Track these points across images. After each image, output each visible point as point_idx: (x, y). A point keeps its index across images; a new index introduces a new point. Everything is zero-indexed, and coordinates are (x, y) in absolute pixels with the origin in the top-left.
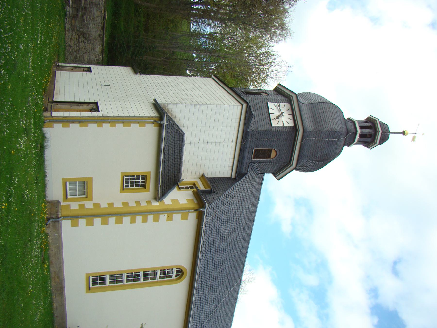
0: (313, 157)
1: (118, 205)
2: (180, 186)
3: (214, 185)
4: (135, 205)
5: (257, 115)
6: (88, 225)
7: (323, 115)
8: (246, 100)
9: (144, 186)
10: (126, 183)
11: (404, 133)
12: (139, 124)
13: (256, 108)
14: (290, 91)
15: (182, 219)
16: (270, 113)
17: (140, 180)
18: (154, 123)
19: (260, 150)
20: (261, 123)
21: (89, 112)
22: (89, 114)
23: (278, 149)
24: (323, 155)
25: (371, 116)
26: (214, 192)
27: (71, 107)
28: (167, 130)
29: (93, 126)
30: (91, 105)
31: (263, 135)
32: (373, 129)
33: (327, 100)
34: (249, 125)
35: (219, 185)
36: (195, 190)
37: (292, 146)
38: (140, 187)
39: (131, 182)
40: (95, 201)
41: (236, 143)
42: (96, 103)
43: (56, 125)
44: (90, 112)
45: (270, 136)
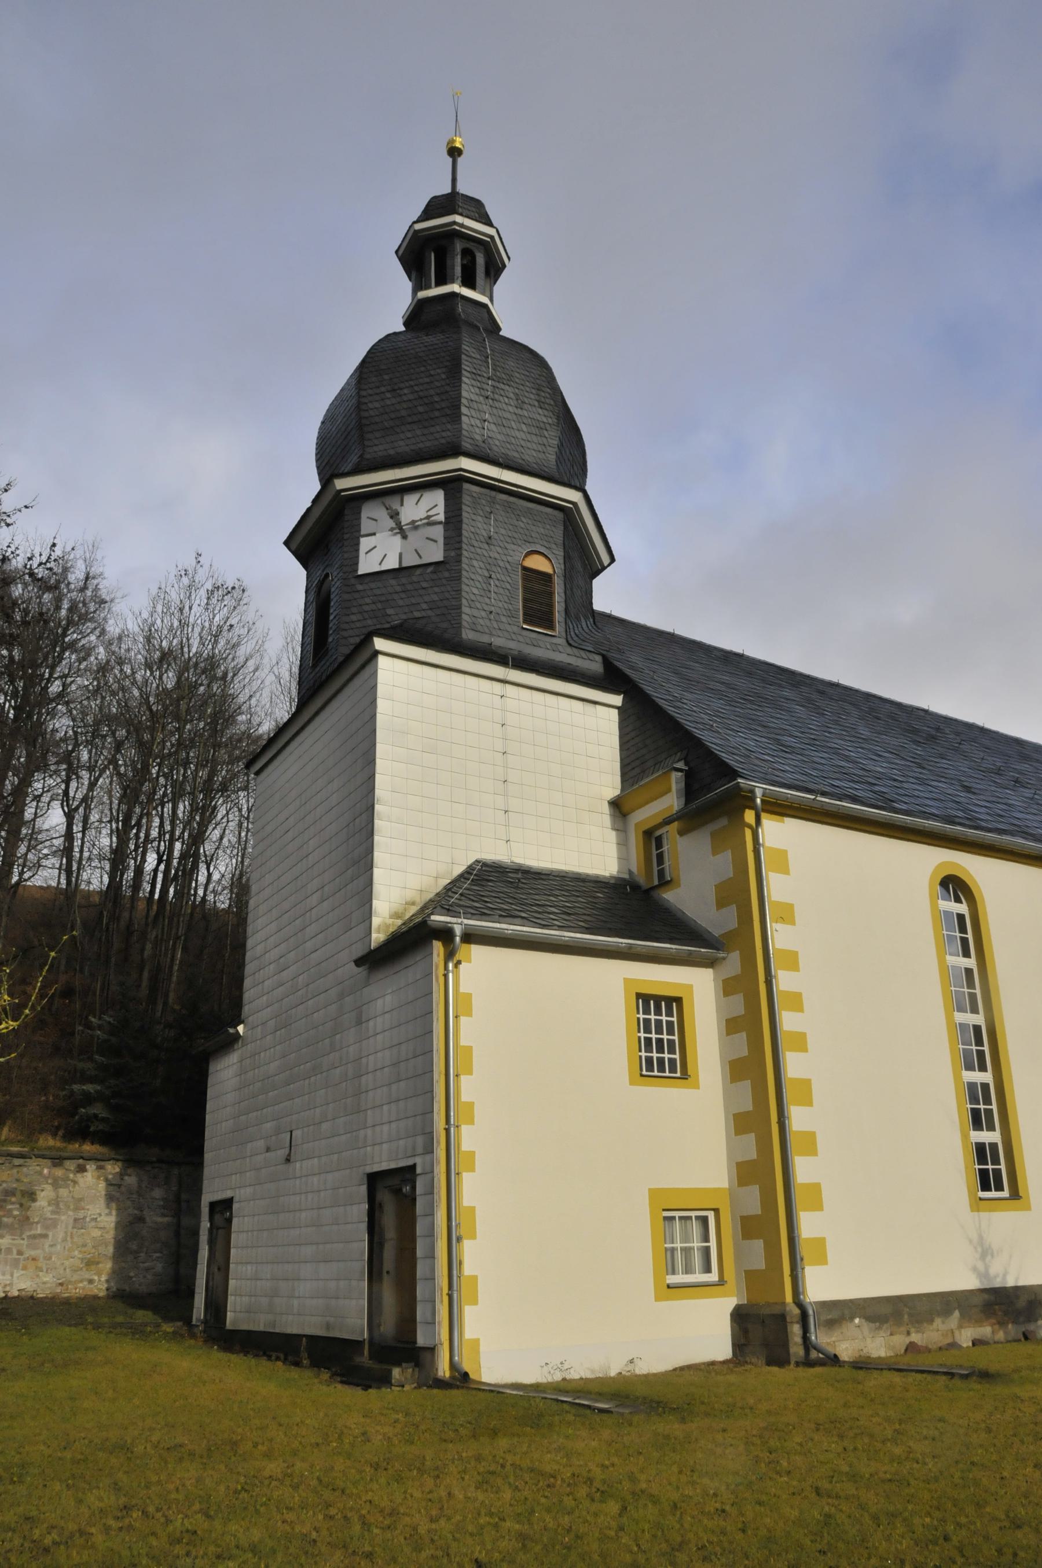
0: (547, 436)
2: (656, 882)
6: (817, 1205)
8: (352, 647)
10: (662, 1069)
14: (314, 501)
16: (397, 566)
18: (459, 962)
19: (524, 607)
23: (523, 546)
24: (538, 401)
25: (397, 252)
27: (388, 1272)
28: (482, 915)
33: (347, 383)
42: (374, 1180)
45: (479, 571)
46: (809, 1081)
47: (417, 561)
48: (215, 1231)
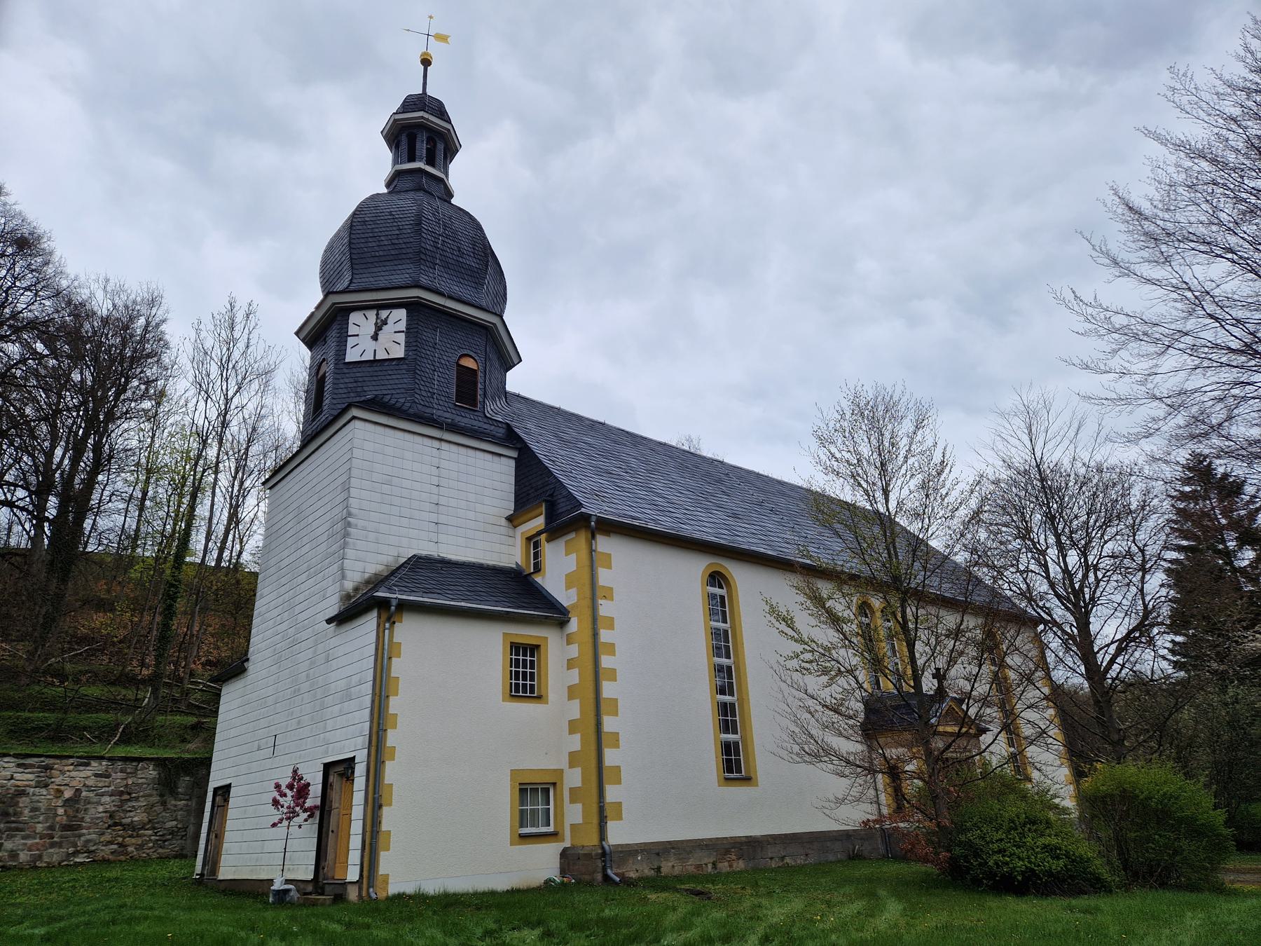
1: (574, 710)
2: (532, 571)
3: (533, 495)
4: (576, 672)
5: (377, 388)
7: (383, 238)
9: (534, 649)
11: (426, 62)
12: (393, 659)
13: (359, 390)
14: (318, 308)
15: (610, 567)
17: (521, 658)
18: (394, 623)
20: (397, 381)
21: (353, 783)
22: (360, 782)
25: (382, 132)
26: (551, 495)
27: (332, 831)
29: (391, 772)
30: (331, 779)
31: (425, 379)
32: (415, 131)
33: (343, 227)
34: (399, 409)
35: (534, 485)
36: (543, 537)
37: (452, 319)
38: (535, 659)
39: (525, 679)
40: (563, 763)
41: (441, 440)
42: (328, 767)
43: (383, 869)
44: (353, 780)
46: (616, 700)
47: (386, 356)
48: (216, 808)
